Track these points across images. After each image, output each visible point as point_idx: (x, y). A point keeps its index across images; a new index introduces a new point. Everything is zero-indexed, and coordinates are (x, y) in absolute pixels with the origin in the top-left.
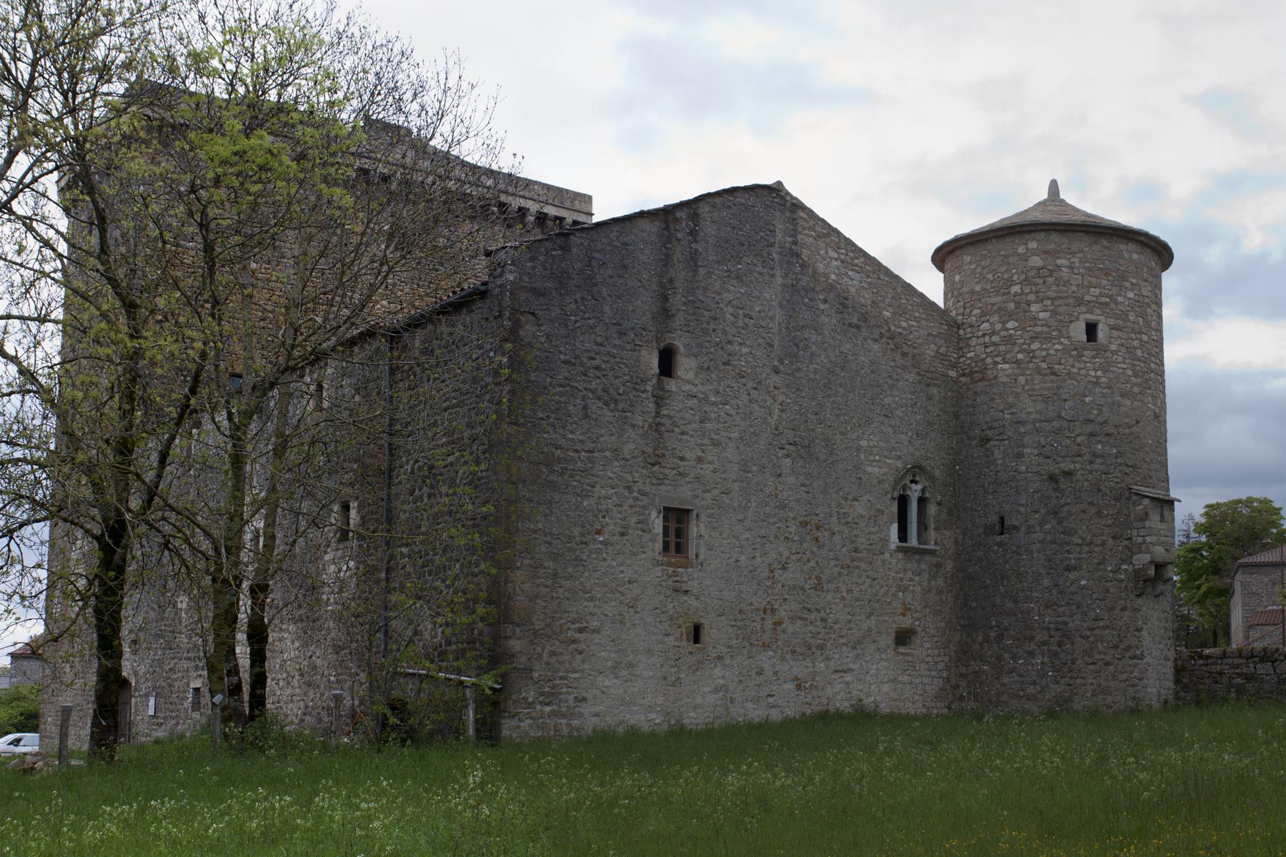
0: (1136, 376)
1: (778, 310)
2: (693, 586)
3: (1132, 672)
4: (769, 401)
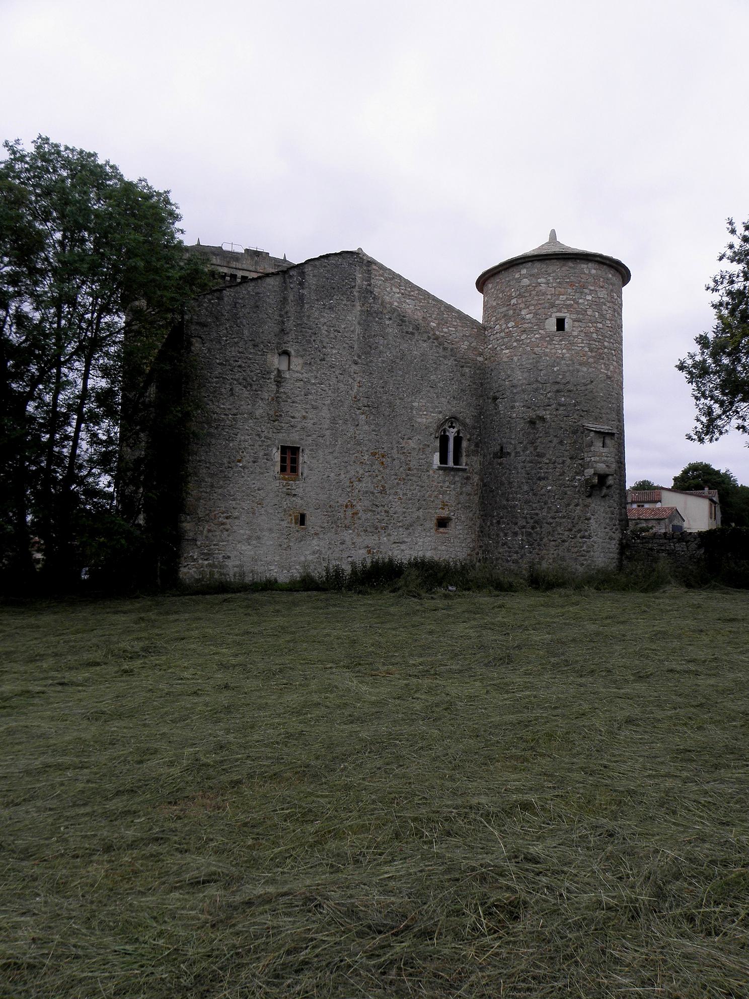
0: (591, 352)
1: (358, 326)
2: (299, 491)
3: (581, 547)
4: (351, 381)
